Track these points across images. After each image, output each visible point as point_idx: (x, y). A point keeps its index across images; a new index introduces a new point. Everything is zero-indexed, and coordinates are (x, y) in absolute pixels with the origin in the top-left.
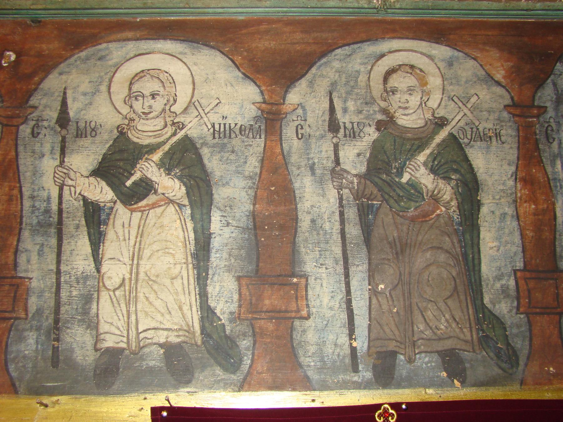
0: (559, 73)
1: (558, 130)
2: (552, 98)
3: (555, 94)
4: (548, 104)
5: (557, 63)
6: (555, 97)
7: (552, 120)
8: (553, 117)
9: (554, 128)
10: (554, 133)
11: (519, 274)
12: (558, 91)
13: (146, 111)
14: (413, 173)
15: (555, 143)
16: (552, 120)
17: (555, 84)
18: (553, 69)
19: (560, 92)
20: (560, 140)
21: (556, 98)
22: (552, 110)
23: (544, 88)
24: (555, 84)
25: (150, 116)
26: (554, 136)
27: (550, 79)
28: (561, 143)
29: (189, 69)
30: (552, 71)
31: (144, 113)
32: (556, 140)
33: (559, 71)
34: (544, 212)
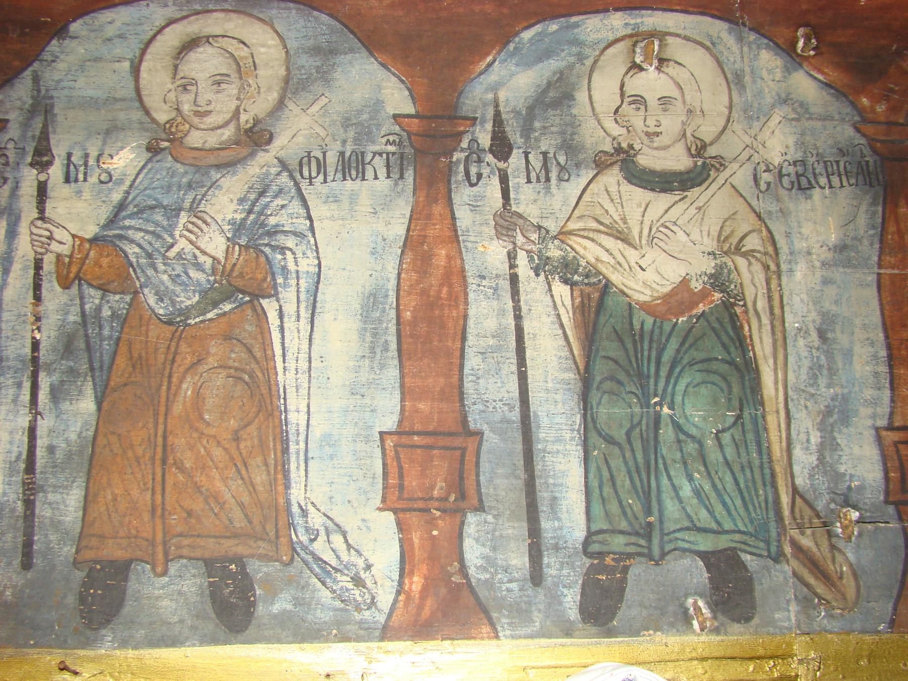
0: (50, 58)
1: (18, 164)
2: (25, 103)
3: (33, 97)
4: (12, 116)
5: (52, 38)
6: (30, 102)
7: (11, 145)
8: (16, 139)
9: (11, 160)
10: (8, 169)
11: (389, 443)
12: (39, 91)
13: (652, 129)
14: (193, 237)
15: (6, 187)
16: (11, 145)
17: (36, 79)
18: (43, 50)
19: (43, 92)
20: (17, 183)
21: (32, 105)
22: (17, 126)
23: (12, 86)
24: (36, 79)
25: (657, 141)
26: (7, 175)
27: (30, 69)
28: (17, 187)
29: (160, 31)
30: (38, 55)
31: (648, 134)
32: (9, 181)
33: (52, 55)
34: (755, 379)
